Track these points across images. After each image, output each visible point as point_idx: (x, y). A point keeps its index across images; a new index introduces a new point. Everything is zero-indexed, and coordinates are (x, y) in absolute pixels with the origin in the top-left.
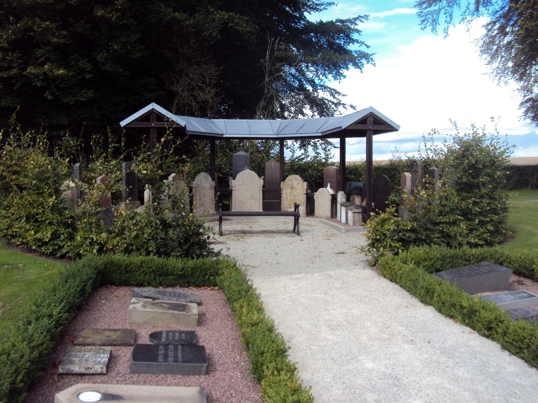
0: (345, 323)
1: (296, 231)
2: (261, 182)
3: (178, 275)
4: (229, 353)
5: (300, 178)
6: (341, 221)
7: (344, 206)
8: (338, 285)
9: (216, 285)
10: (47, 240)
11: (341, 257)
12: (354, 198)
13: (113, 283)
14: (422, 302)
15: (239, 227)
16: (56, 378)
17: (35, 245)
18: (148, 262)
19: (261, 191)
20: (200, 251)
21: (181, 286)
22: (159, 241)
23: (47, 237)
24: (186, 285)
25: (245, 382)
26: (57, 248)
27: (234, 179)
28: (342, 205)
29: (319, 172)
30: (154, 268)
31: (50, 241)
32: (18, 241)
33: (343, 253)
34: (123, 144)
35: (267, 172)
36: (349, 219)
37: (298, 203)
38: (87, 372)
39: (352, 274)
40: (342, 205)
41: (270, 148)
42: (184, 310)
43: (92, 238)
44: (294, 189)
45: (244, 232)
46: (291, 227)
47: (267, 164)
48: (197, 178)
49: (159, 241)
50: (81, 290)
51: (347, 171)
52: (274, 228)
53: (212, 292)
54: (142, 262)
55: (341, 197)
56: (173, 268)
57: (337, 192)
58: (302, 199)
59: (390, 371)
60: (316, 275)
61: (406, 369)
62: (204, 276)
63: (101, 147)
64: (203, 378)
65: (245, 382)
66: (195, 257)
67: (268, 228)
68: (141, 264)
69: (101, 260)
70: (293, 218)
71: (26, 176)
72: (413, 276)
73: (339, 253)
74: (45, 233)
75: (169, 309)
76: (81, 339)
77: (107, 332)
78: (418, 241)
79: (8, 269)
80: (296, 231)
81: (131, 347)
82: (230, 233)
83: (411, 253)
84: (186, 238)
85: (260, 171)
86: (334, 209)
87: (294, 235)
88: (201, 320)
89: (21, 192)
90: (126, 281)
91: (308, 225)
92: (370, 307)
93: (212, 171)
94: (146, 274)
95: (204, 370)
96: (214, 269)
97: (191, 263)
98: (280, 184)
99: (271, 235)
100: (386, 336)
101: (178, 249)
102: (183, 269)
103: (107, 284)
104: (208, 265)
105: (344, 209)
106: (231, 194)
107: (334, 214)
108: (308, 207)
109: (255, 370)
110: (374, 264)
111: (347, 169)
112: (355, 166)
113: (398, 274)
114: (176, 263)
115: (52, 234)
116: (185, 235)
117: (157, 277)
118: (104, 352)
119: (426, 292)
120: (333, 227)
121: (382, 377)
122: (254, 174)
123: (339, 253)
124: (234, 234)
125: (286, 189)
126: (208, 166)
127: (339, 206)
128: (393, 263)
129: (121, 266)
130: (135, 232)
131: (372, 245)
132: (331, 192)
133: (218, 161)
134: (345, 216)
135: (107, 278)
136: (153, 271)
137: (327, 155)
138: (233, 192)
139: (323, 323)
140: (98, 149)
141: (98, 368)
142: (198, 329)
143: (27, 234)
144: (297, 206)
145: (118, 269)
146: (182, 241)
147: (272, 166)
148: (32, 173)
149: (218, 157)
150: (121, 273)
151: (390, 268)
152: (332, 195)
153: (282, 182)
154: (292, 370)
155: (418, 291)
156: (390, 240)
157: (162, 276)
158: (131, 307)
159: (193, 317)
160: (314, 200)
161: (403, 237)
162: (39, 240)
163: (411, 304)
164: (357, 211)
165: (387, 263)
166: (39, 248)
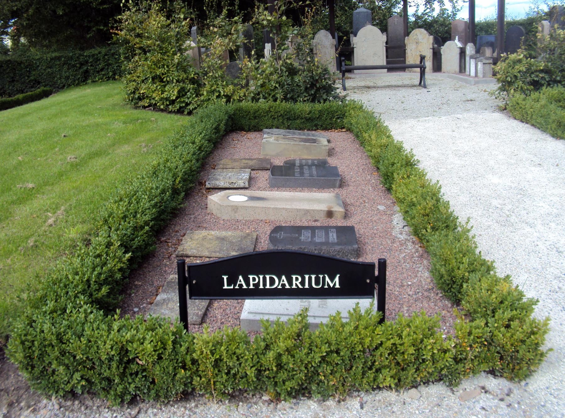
0: (472, 152)
1: (422, 84)
2: (384, 38)
3: (306, 118)
4: (360, 174)
5: (425, 32)
6: (470, 75)
7: (472, 58)
8: (466, 125)
9: (344, 128)
10: (174, 98)
11: (469, 105)
12: (485, 50)
13: (242, 129)
14: (553, 136)
15: (363, 84)
16: (204, 192)
17: (163, 104)
18: (276, 107)
19: (385, 48)
20: (327, 95)
21: (309, 130)
22: (286, 86)
23: (174, 95)
24: (314, 128)
25: (376, 193)
26: (184, 105)
27: (355, 36)
28: (471, 57)
29: (446, 26)
30: (282, 112)
31: (177, 98)
32: (146, 103)
33: (471, 100)
34: (237, 7)
35: (390, 28)
36: (479, 72)
37: (423, 54)
38: (231, 186)
39: (481, 116)
40: (471, 57)
41: (392, 6)
42: (315, 143)
43: (219, 91)
44: (419, 44)
45: (369, 87)
46: (417, 82)
47: (390, 21)
48: (317, 36)
49: (286, 86)
50: (215, 129)
51: (478, 28)
52: (400, 83)
53: (340, 134)
54: (270, 107)
55: (470, 49)
56: (300, 112)
57: (465, 44)
58: (429, 54)
59: (516, 185)
60: (443, 118)
61: (532, 183)
62: (331, 119)
63: (215, 11)
64: (337, 190)
65: (376, 193)
66: (322, 101)
67: (393, 83)
68: (269, 109)
69: (231, 107)
70: (418, 69)
71: (148, 38)
72: (544, 111)
73: (468, 101)
74: (171, 92)
75: (300, 141)
76: (221, 166)
77: (244, 161)
78: (552, 82)
79: (142, 122)
80: (422, 84)
81: (268, 171)
82: (354, 88)
83: (544, 94)
84: (312, 83)
85: (384, 29)
86: (463, 61)
87: (420, 88)
88: (331, 152)
89: (145, 54)
90: (255, 127)
91: (435, 80)
92: (498, 141)
93: (332, 29)
94: (274, 118)
95: (338, 183)
96: (341, 111)
97: (318, 106)
98: (404, 40)
99: (396, 89)
100: (513, 161)
101: (305, 94)
102: (310, 112)
103: (237, 130)
104: (335, 108)
105: (473, 62)
106: (353, 52)
107: (462, 69)
108: (435, 63)
109: (386, 180)
110: (503, 109)
111: (477, 26)
112: (486, 22)
113: (529, 112)
114: (304, 107)
115: (179, 92)
116: (311, 80)
117: (285, 122)
118: (244, 172)
119: (557, 126)
120: (461, 80)
121: (508, 188)
122: (376, 30)
123: (468, 101)
124: (358, 89)
125: (411, 45)
126: (327, 25)
127: (467, 59)
128: (524, 103)
129: (249, 112)
130: (261, 80)
131: (502, 89)
132: (460, 45)
133: (337, 21)
134: (474, 68)
135: (238, 124)
136: (281, 115)
137: (454, 7)
138: (355, 49)
139: (450, 152)
140: (212, 13)
141: (241, 184)
142: (329, 158)
143: (154, 95)
144: (422, 58)
145: (247, 115)
146: (309, 86)
147: (395, 23)
148: (155, 34)
149: (337, 17)
150: (250, 119)
151: (521, 108)
152: (461, 48)
153: (406, 38)
154: (422, 175)
155: (549, 127)
156: (521, 82)
157: (290, 120)
158: (264, 140)
159: (324, 148)
160: (441, 55)
161: (536, 79)
162: (167, 99)
163: (541, 139)
164: (487, 62)
165: (518, 104)
166: (168, 106)
